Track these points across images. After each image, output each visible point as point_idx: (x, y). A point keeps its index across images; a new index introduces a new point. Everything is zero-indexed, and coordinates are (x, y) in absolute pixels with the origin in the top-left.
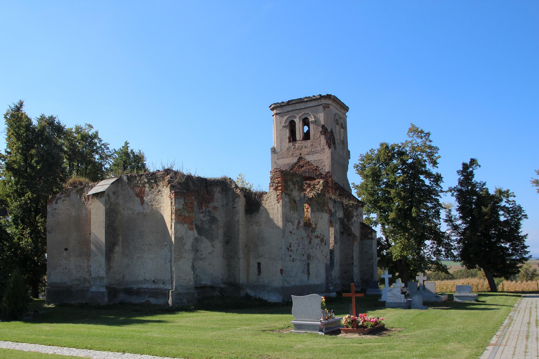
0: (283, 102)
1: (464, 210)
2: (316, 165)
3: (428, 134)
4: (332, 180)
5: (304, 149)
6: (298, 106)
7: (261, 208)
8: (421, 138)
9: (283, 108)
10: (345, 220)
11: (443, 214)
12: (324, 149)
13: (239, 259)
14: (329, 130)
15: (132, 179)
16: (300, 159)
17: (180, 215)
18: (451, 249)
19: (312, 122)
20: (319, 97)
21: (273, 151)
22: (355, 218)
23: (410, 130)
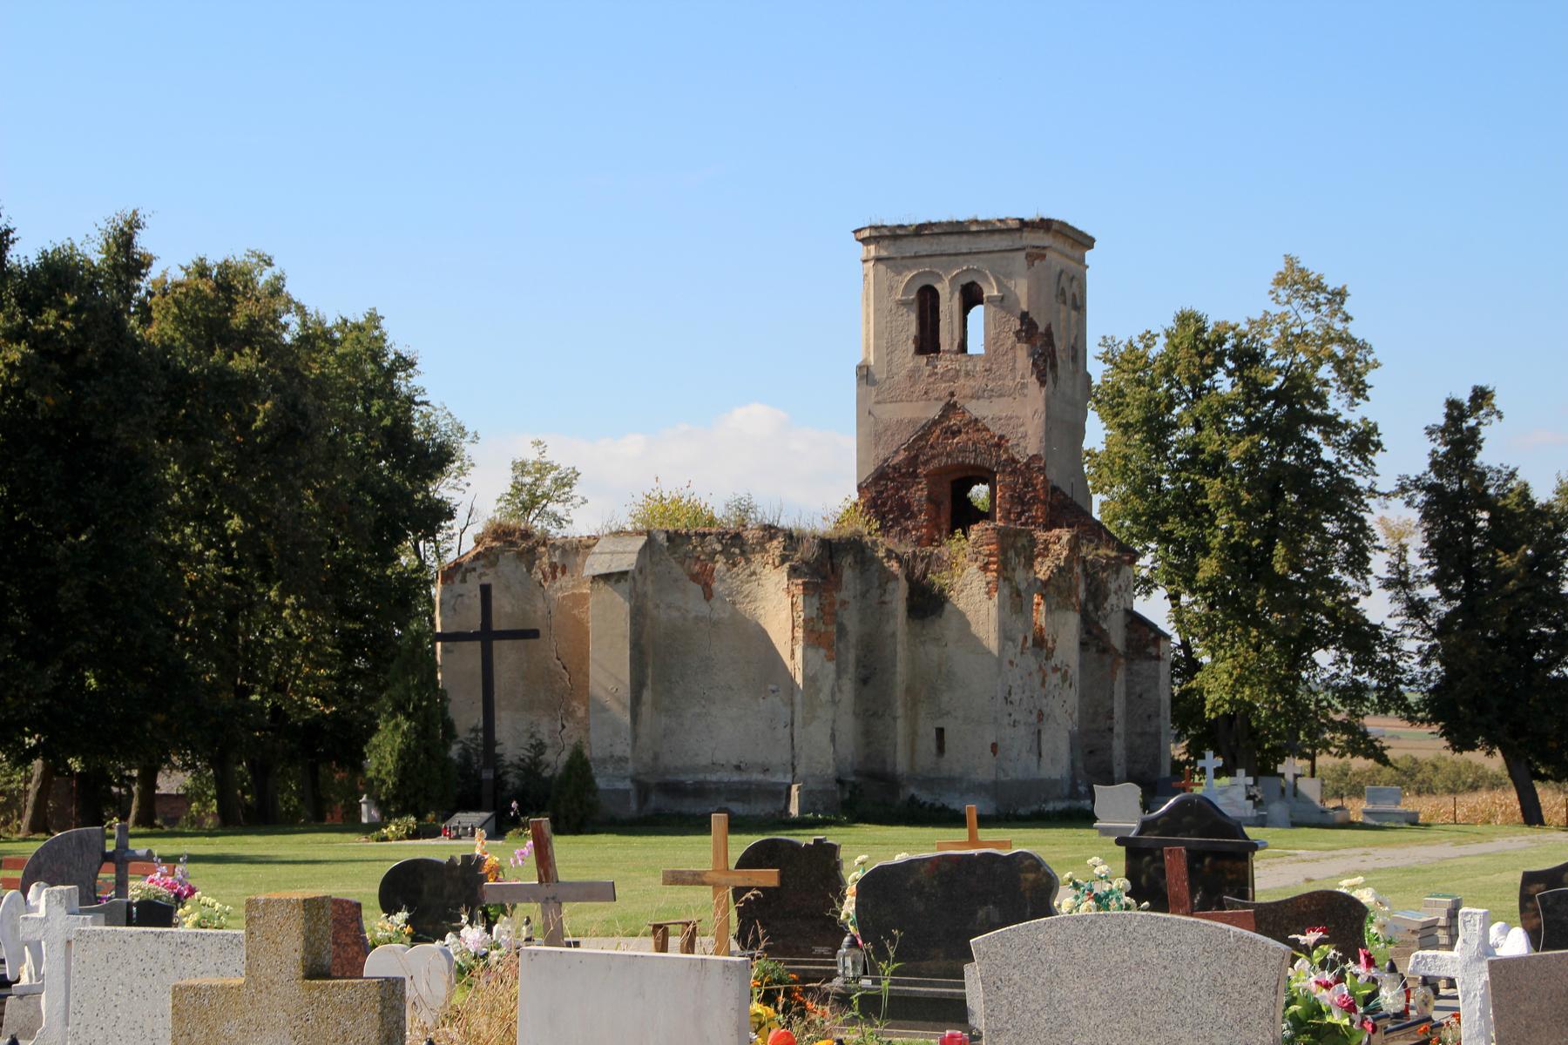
0: (901, 227)
1: (1450, 552)
2: (1000, 433)
3: (1340, 295)
4: (1046, 480)
5: (962, 381)
6: (950, 244)
7: (947, 606)
8: (1316, 307)
9: (899, 243)
10: (1090, 607)
11: (1379, 564)
12: (1024, 386)
13: (895, 719)
14: (1042, 329)
15: (678, 540)
16: (950, 408)
17: (812, 631)
18: (1400, 681)
19: (991, 300)
20: (1015, 225)
21: (865, 374)
22: (1113, 599)
23: (1281, 281)
